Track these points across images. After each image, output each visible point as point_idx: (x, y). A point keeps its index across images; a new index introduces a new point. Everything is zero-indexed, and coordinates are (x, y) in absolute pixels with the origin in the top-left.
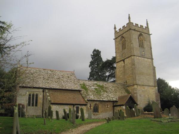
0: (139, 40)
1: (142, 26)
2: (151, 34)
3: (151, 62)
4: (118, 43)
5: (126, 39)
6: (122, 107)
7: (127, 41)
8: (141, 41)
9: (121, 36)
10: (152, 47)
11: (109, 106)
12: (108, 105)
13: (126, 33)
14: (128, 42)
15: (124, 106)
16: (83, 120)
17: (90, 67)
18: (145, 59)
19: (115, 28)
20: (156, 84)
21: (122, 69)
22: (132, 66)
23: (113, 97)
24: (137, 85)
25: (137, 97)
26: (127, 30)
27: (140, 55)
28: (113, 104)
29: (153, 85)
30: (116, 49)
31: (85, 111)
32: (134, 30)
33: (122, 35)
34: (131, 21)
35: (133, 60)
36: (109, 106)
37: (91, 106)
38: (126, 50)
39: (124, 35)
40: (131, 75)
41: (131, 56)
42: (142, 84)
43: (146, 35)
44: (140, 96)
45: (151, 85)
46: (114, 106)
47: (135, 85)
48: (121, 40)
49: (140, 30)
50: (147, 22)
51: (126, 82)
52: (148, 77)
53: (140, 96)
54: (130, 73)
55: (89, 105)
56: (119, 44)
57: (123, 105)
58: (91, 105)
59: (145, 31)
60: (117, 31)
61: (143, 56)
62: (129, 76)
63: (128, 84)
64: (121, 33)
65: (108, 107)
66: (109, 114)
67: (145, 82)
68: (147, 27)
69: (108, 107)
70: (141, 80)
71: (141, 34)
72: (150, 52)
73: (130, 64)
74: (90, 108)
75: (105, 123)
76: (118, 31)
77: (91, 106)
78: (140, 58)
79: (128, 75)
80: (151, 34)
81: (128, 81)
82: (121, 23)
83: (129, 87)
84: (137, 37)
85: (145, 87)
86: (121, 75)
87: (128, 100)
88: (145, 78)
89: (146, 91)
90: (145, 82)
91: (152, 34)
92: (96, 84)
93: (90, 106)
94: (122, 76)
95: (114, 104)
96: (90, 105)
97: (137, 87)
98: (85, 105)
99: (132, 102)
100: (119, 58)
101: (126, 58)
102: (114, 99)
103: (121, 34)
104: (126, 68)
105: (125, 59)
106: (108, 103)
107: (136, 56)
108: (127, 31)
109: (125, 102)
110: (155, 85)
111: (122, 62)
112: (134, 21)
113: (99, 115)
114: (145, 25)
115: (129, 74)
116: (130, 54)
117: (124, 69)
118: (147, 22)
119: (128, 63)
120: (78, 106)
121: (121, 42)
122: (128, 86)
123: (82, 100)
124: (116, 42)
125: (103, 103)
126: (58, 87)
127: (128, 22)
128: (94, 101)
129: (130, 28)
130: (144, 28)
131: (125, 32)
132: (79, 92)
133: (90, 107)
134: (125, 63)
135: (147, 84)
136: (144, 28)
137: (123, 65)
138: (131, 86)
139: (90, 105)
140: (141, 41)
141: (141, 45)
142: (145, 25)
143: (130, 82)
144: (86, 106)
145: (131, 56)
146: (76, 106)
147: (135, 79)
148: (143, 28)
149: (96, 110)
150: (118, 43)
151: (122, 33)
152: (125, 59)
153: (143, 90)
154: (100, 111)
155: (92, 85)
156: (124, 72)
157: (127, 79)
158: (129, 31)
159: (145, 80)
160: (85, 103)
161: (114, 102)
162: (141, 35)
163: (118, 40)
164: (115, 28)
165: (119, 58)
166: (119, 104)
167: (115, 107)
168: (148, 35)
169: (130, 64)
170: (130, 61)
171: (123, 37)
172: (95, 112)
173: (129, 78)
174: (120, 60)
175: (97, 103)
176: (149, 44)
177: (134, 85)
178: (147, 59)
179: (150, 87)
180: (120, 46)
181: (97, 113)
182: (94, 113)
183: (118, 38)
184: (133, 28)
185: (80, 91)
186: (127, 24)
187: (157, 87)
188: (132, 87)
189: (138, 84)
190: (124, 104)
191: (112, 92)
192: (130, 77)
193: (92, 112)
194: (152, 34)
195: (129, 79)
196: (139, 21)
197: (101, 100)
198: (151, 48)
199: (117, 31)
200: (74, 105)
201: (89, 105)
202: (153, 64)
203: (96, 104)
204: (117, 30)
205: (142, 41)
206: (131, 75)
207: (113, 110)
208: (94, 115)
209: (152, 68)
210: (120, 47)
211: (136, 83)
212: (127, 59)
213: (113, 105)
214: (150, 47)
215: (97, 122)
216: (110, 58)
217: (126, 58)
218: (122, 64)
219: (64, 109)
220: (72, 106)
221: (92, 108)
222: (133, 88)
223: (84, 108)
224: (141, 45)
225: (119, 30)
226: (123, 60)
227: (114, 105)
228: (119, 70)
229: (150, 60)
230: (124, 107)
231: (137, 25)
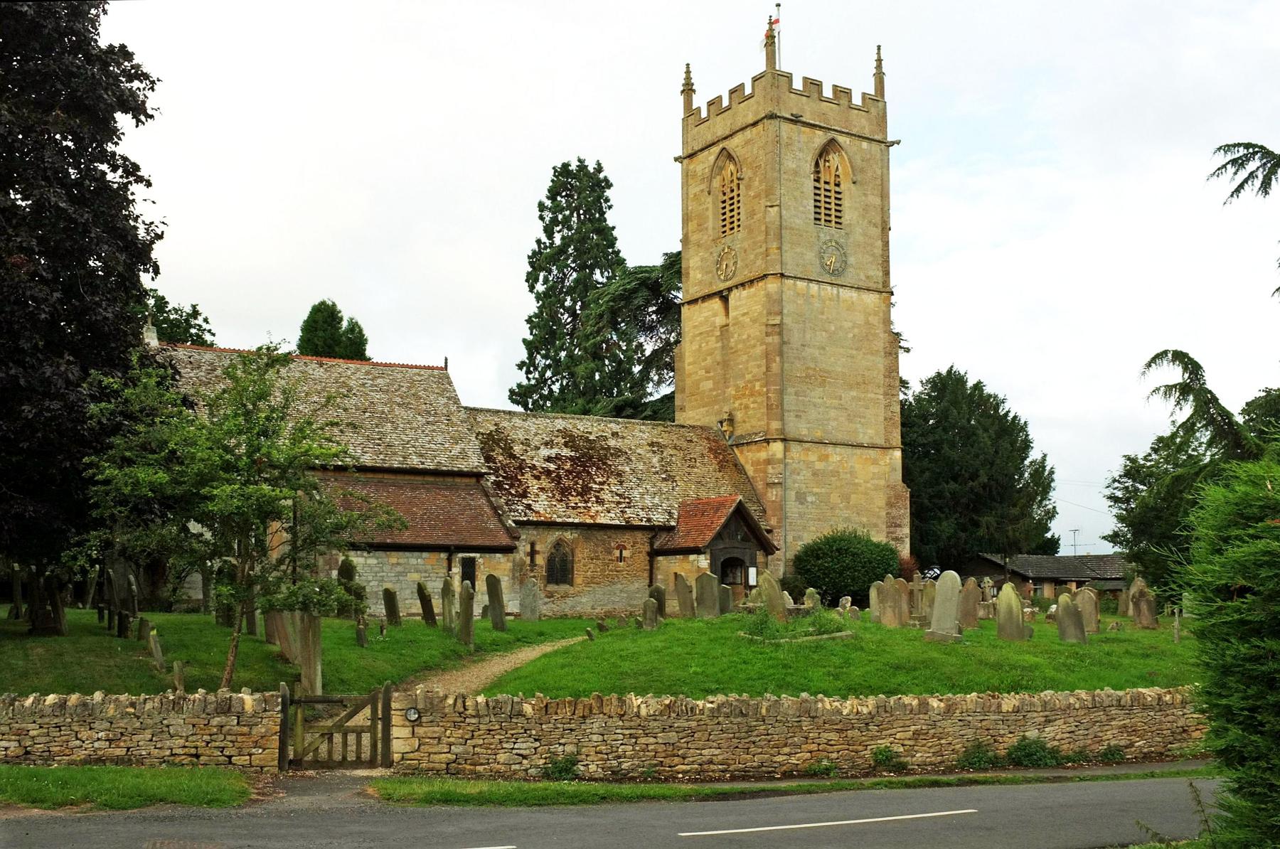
0: (817, 180)
1: (842, 93)
2: (893, 144)
3: (876, 314)
4: (703, 186)
5: (747, 173)
6: (692, 557)
7: (748, 187)
8: (832, 187)
9: (715, 150)
10: (892, 224)
11: (626, 553)
12: (622, 548)
13: (748, 133)
14: (752, 193)
15: (702, 557)
16: (499, 625)
17: (531, 279)
18: (846, 294)
19: (688, 90)
20: (896, 438)
21: (713, 343)
22: (767, 335)
23: (653, 503)
24: (784, 440)
25: (781, 507)
26: (750, 120)
27: (819, 269)
28: (652, 544)
29: (880, 441)
30: (686, 219)
31: (505, 583)
32: (795, 120)
33: (728, 144)
34: (784, 65)
35: (775, 305)
36: (625, 553)
37: (538, 552)
38: (740, 235)
39: (733, 144)
40: (757, 386)
41: (765, 276)
42: (818, 434)
43: (865, 145)
44: (801, 498)
45: (865, 440)
46: (653, 554)
47: (775, 440)
48: (717, 169)
49: (833, 115)
50: (879, 61)
51: (731, 421)
52: (854, 393)
53: (801, 498)
54: (755, 370)
55: (524, 548)
56: (702, 191)
57: (697, 551)
58: (538, 548)
59: (862, 124)
60: (699, 109)
61: (835, 275)
62: (745, 387)
63: (738, 432)
64: (720, 126)
65: (621, 558)
66: (630, 593)
67: (834, 424)
68: (876, 99)
69: (621, 558)
70: (814, 412)
71: (833, 141)
72: (878, 251)
73: (754, 321)
74: (532, 560)
75: (580, 638)
76: (704, 114)
77: (538, 552)
78: (814, 287)
79: (741, 384)
80: (893, 144)
81: (739, 416)
82: (728, 68)
83: (745, 448)
84: (809, 167)
85: (830, 449)
86: (708, 379)
87: (725, 526)
88: (836, 402)
89: (835, 473)
90: (834, 424)
91: (898, 143)
92: (564, 433)
93: (533, 553)
94: (709, 384)
95: (659, 541)
96: (528, 548)
97: (786, 450)
98: (508, 550)
99: (743, 535)
100: (699, 276)
101: (736, 287)
102: (659, 518)
103: (721, 132)
104: (732, 342)
105: (730, 289)
106: (626, 538)
107: (789, 277)
108: (755, 124)
109: (709, 536)
110: (887, 440)
111: (716, 304)
112: (797, 62)
113: (574, 595)
114: (861, 85)
115: (748, 377)
116: (759, 262)
117: (723, 347)
118: (879, 61)
119: (744, 315)
120: (472, 555)
121: (716, 183)
122: (737, 446)
123: (493, 524)
124: (687, 177)
125: (600, 535)
126: (367, 456)
127: (761, 67)
128: (550, 525)
129: (776, 100)
130: (857, 100)
131: (739, 125)
132: (473, 480)
133: (528, 560)
134: (732, 314)
135: (840, 437)
136: (857, 100)
137: (720, 320)
138: (754, 447)
139: (533, 545)
140: (832, 187)
141: (827, 209)
142: (861, 85)
143: (751, 420)
144: (511, 556)
145: (765, 276)
146: (460, 555)
147: (776, 409)
148: (851, 107)
149: (559, 571)
150: (703, 186)
151: (727, 133)
152: (730, 289)
153: (819, 466)
154: (578, 580)
155: (539, 437)
156: (725, 364)
157: (736, 405)
158: (760, 126)
159: (833, 413)
160: (504, 540)
161: (654, 530)
162: (824, 152)
163: (699, 168)
164: (688, 90)
165: (699, 276)
166: (680, 541)
167: (660, 558)
168: (874, 145)
169: (754, 321)
170: (758, 308)
171: (728, 156)
172: (557, 583)
173: (744, 401)
174: (707, 291)
175: (568, 535)
176: (878, 201)
177: (767, 441)
178: (854, 294)
179: (858, 451)
180: (710, 206)
181: (564, 588)
182: (551, 587)
183: (701, 156)
184: (791, 106)
185: (479, 476)
186: (755, 80)
187: (898, 454)
188: (759, 451)
189: (791, 436)
190: (707, 547)
191: (651, 481)
192: (752, 395)
193: (540, 584)
194: (898, 143)
195: (747, 407)
196: (825, 56)
197: (589, 521)
198: (885, 228)
199: (699, 109)
200: (451, 550)
201: (524, 548)
202: (888, 322)
203: (558, 544)
204: (700, 101)
205: (838, 185)
206: (757, 386)
207: (646, 574)
208: (550, 595)
209: (881, 342)
210: (710, 214)
211: (782, 431)
212: (744, 293)
213: (647, 548)
214: (878, 220)
215: (541, 636)
216: (655, 259)
217: (736, 287)
218: (715, 315)
219: (419, 585)
220: (443, 555)
221: (540, 560)
222: (763, 455)
223: (500, 566)
224: (827, 209)
225: (710, 104)
226: (723, 296)
227: (657, 545)
228: (695, 347)
229: (871, 299)
230: (703, 562)
231: (813, 85)
